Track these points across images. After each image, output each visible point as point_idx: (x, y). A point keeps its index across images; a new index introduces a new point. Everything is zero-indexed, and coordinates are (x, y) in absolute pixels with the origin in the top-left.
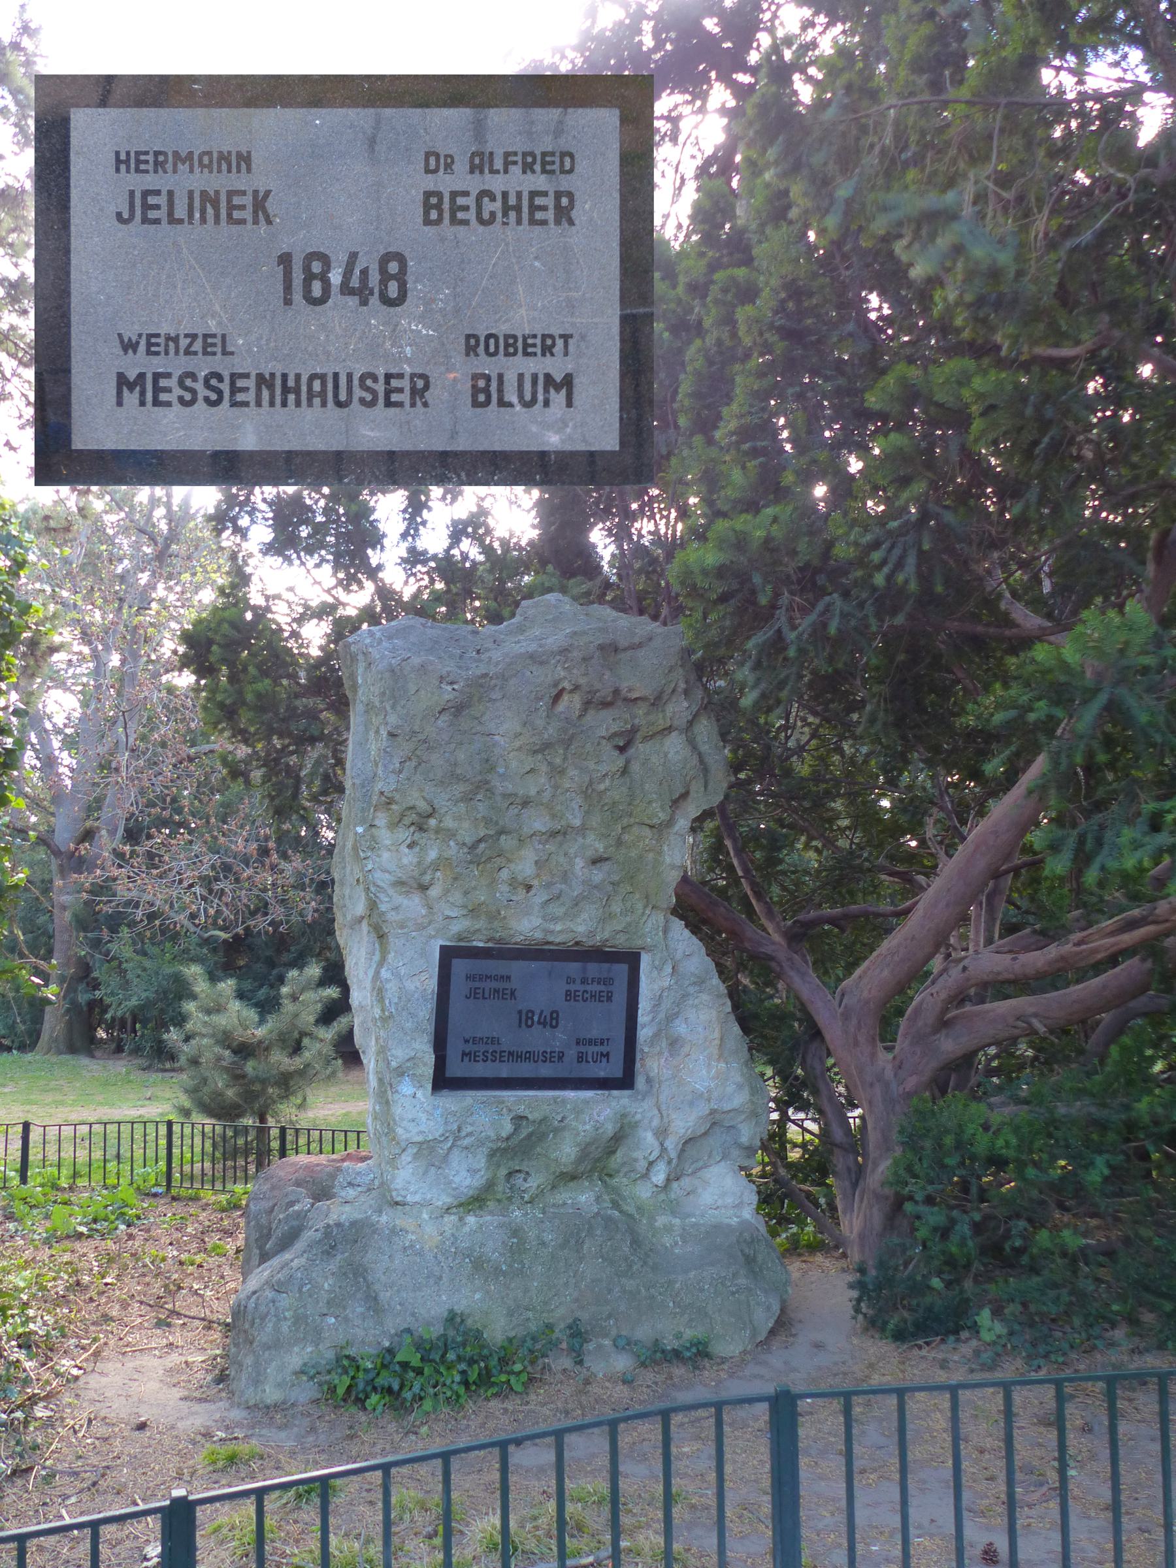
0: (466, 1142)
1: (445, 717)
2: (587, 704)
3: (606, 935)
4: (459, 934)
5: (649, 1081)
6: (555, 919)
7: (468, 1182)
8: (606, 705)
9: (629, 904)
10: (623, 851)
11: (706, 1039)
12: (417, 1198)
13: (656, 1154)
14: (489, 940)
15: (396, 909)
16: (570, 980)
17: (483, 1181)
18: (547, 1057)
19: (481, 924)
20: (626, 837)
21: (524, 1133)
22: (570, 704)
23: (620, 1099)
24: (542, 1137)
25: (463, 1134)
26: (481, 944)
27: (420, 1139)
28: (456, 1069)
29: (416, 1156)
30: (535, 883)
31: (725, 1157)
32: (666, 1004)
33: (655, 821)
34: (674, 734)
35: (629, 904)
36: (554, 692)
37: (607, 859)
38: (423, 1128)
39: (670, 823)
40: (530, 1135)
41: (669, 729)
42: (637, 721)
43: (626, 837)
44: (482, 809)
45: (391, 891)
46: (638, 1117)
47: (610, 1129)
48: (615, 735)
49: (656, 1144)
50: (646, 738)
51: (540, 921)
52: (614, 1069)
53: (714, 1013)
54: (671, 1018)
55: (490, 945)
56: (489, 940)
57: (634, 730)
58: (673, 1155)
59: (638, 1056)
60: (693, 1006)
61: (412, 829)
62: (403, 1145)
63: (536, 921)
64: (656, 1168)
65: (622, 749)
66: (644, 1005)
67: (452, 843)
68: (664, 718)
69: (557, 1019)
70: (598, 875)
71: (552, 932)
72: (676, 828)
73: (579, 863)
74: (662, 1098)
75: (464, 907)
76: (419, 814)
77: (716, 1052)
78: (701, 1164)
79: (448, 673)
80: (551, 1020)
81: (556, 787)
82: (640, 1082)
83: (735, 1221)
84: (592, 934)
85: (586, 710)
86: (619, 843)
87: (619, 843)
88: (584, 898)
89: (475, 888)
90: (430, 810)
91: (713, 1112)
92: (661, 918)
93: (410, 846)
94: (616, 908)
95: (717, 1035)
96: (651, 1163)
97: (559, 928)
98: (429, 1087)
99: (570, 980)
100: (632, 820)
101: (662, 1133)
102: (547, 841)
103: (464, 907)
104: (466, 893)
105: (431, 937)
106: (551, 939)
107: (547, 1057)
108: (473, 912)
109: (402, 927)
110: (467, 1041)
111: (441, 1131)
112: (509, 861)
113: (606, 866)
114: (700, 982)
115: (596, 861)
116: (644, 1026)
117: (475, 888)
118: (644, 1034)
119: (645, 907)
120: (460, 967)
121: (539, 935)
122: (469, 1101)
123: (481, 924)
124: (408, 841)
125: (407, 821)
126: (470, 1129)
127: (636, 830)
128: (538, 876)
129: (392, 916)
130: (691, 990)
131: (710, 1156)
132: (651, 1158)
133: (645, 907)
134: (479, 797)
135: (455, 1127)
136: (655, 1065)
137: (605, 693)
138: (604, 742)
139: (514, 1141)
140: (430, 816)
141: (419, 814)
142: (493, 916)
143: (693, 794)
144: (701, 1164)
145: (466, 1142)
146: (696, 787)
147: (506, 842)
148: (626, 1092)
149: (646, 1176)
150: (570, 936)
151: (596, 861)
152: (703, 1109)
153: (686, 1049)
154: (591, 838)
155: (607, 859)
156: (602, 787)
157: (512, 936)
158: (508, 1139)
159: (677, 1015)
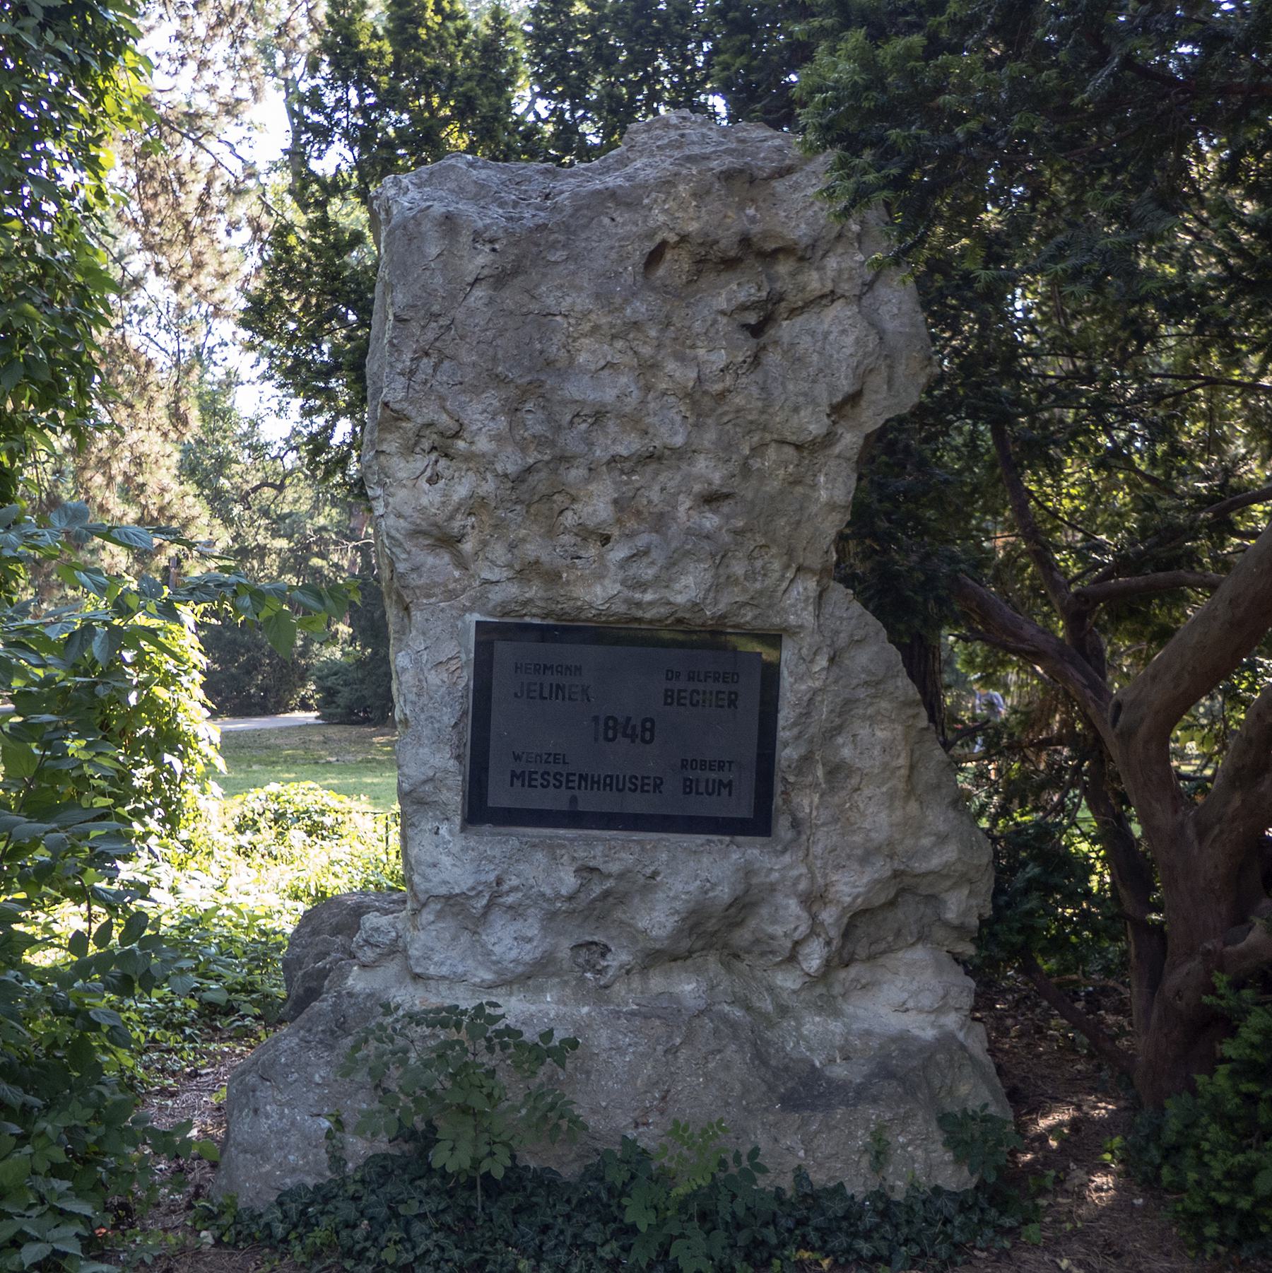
0: (510, 900)
1: (480, 292)
2: (701, 264)
3: (722, 607)
4: (503, 604)
5: (796, 824)
6: (642, 586)
7: (513, 954)
8: (729, 264)
9: (759, 564)
10: (754, 482)
11: (885, 766)
12: (444, 970)
13: (803, 929)
14: (546, 616)
15: (415, 569)
16: (671, 675)
17: (538, 954)
18: (638, 785)
19: (534, 591)
20: (756, 464)
21: (597, 890)
22: (675, 267)
23: (751, 851)
24: (622, 899)
25: (505, 887)
26: (537, 621)
27: (443, 890)
28: (500, 795)
29: (440, 915)
30: (615, 532)
31: (922, 938)
32: (823, 711)
33: (804, 438)
34: (839, 304)
35: (759, 564)
36: (649, 246)
37: (727, 496)
38: (445, 876)
39: (829, 439)
40: (606, 894)
41: (831, 297)
42: (778, 286)
43: (756, 464)
44: (534, 423)
45: (408, 545)
46: (775, 876)
47: (724, 893)
48: (744, 308)
49: (805, 915)
50: (793, 312)
51: (618, 587)
52: (744, 809)
53: (899, 728)
54: (832, 732)
55: (550, 622)
56: (546, 616)
57: (776, 299)
58: (834, 933)
59: (779, 788)
60: (864, 718)
61: (434, 456)
62: (422, 897)
63: (614, 588)
64: (805, 950)
65: (756, 331)
66: (786, 714)
67: (489, 476)
68: (821, 279)
69: (652, 730)
70: (710, 521)
71: (639, 605)
72: (837, 450)
73: (685, 503)
74: (818, 849)
75: (509, 566)
76: (442, 434)
77: (901, 786)
78: (883, 946)
79: (487, 227)
80: (644, 731)
81: (648, 388)
82: (782, 826)
83: (929, 1034)
84: (695, 606)
85: (699, 272)
86: (746, 471)
87: (746, 471)
88: (687, 553)
89: (523, 540)
90: (455, 427)
91: (896, 874)
92: (812, 584)
93: (431, 481)
94: (738, 568)
95: (902, 761)
96: (797, 944)
97: (649, 597)
98: (458, 820)
99: (671, 675)
100: (768, 437)
101: (813, 899)
102: (633, 471)
103: (509, 566)
104: (512, 547)
105: (466, 610)
106: (640, 614)
107: (638, 785)
108: (526, 571)
109: (428, 596)
110: (517, 758)
111: (470, 883)
112: (574, 500)
113: (726, 508)
114: (876, 684)
115: (711, 499)
116: (786, 745)
117: (523, 540)
118: (787, 754)
119: (787, 567)
120: (503, 650)
121: (620, 608)
122: (514, 842)
123: (534, 591)
124: (428, 473)
125: (426, 444)
126: (515, 881)
127: (772, 452)
128: (619, 521)
129: (414, 579)
130: (862, 693)
131: (898, 934)
132: (796, 936)
133: (787, 567)
134: (529, 406)
135: (492, 877)
136: (806, 802)
137: (727, 243)
138: (723, 320)
139: (583, 899)
140: (456, 435)
141: (442, 434)
142: (552, 577)
143: (868, 397)
144: (883, 946)
145: (510, 900)
146: (877, 381)
147: (575, 474)
148: (759, 840)
149: (792, 958)
150: (663, 610)
151: (711, 499)
152: (880, 868)
153: (854, 781)
154: (702, 465)
155: (727, 496)
156: (718, 387)
157: (580, 609)
158: (571, 898)
159: (839, 729)
